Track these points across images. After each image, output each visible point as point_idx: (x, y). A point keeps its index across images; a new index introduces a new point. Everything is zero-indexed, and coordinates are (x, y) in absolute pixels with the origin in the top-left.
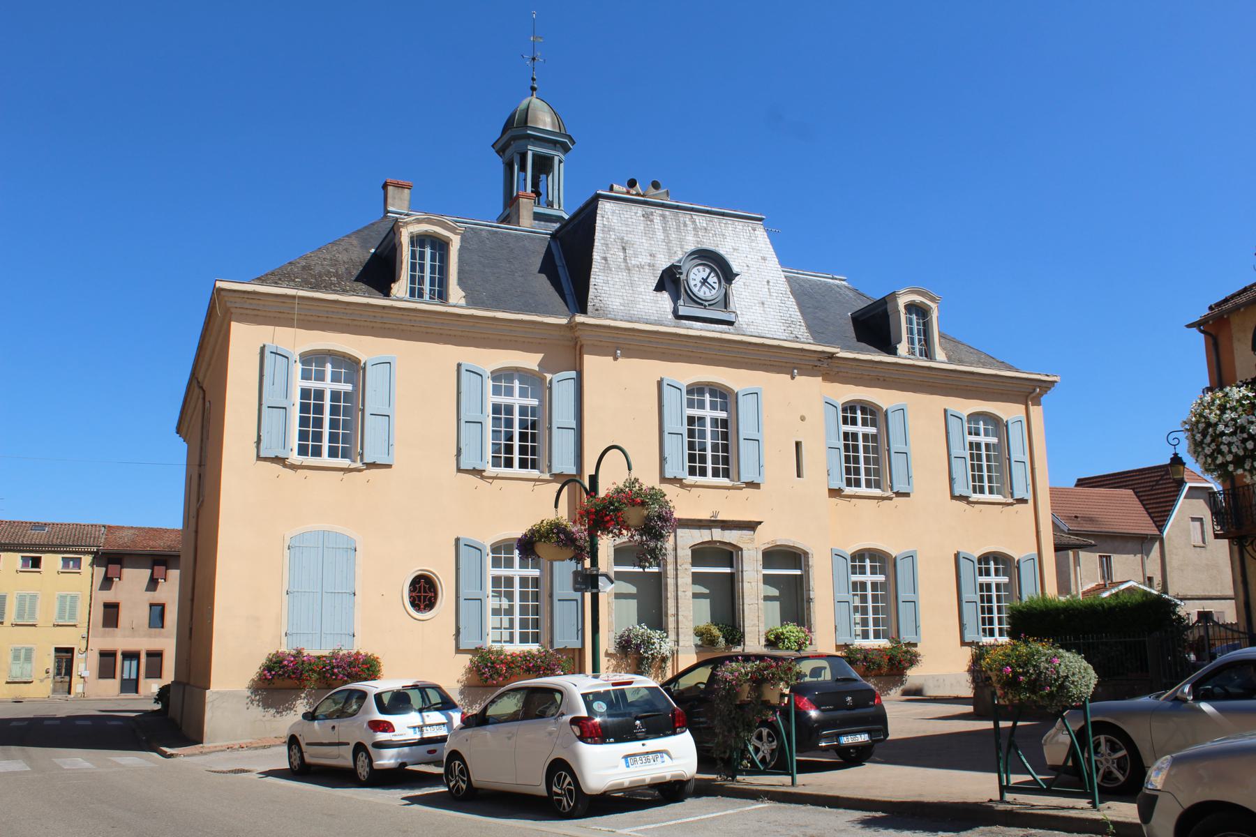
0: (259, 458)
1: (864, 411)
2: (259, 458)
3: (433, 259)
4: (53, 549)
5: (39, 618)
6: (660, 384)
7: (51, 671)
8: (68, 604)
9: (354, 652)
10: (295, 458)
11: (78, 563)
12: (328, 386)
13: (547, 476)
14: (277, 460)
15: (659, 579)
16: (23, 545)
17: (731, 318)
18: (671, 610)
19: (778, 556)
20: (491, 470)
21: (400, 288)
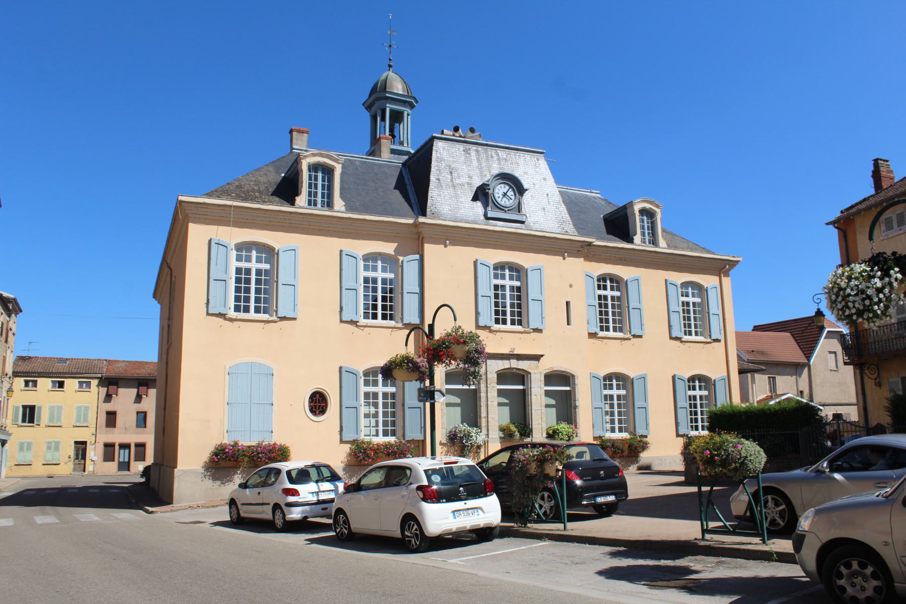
0: (208, 314)
1: (612, 281)
3: (323, 180)
4: (72, 375)
5: (64, 421)
6: (475, 263)
8: (82, 412)
9: (272, 443)
10: (232, 314)
11: (89, 385)
15: (475, 394)
16: (52, 373)
18: (483, 414)
19: (553, 378)
20: (363, 321)
21: (302, 200)
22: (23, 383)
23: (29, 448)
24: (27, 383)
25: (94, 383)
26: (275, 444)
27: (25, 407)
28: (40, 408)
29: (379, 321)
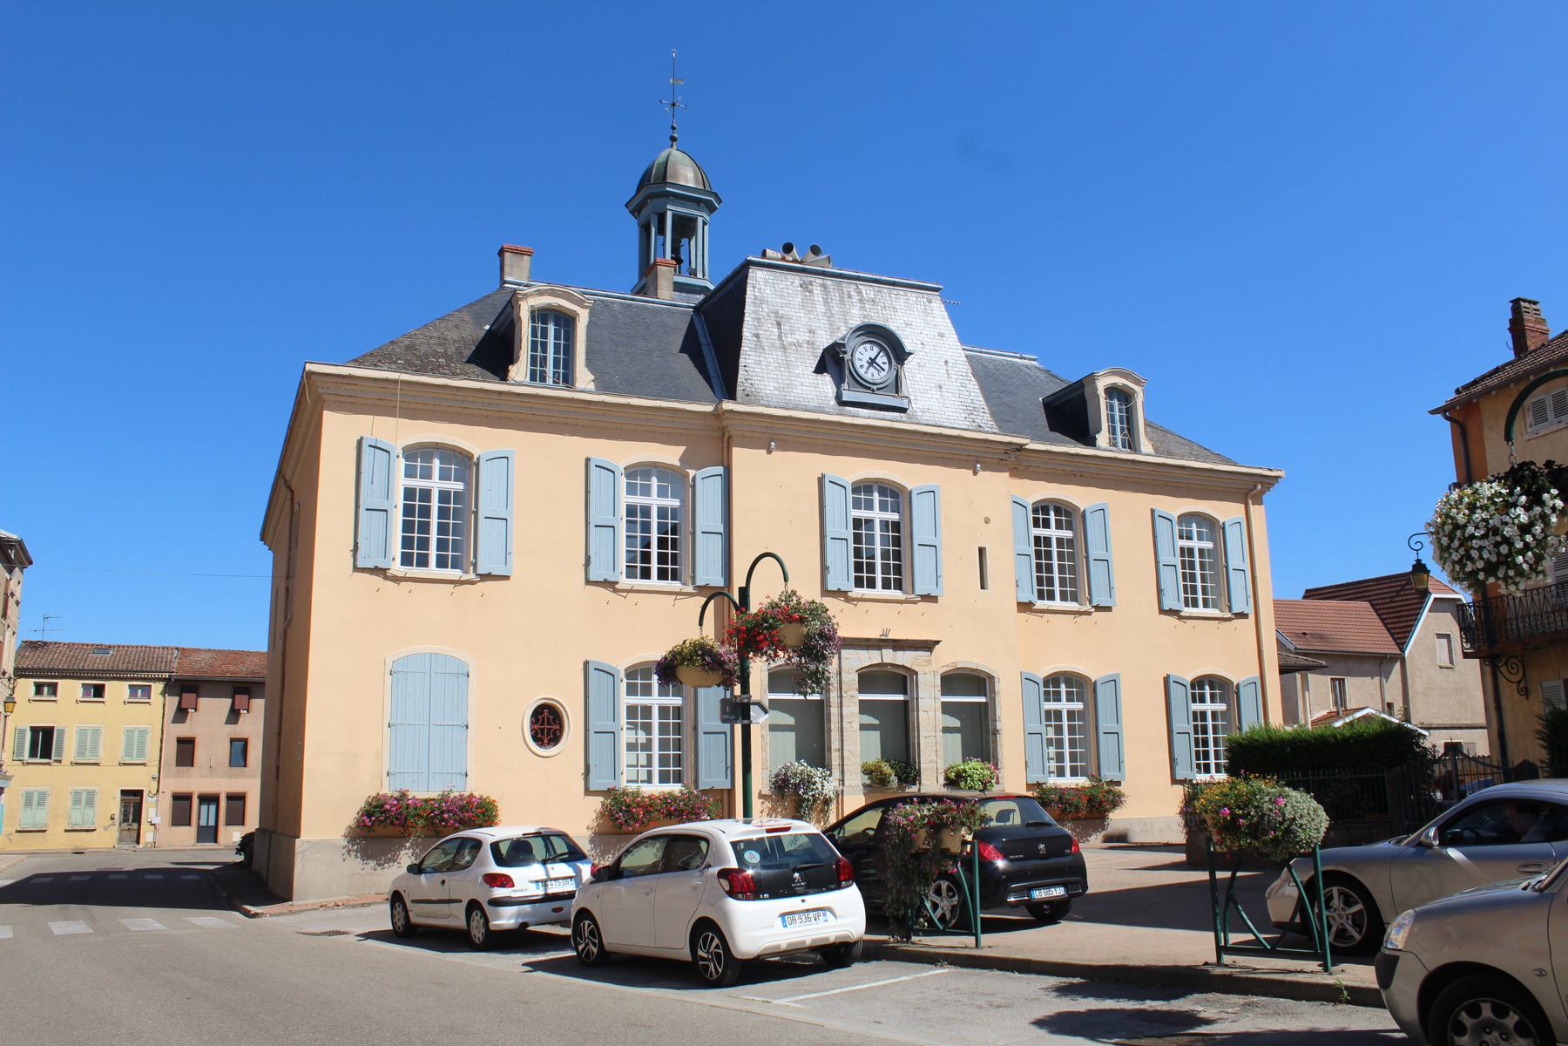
1: (1058, 511)
3: (557, 337)
4: (118, 675)
5: (103, 755)
6: (821, 480)
8: (135, 740)
9: (466, 794)
10: (397, 568)
11: (147, 691)
12: (436, 485)
13: (690, 589)
15: (821, 708)
16: (84, 670)
17: (904, 404)
18: (835, 745)
19: (956, 680)
20: (625, 582)
21: (519, 371)
23: (41, 803)
24: (39, 689)
25: (157, 688)
26: (471, 796)
27: (35, 730)
28: (62, 732)
29: (432, 570)
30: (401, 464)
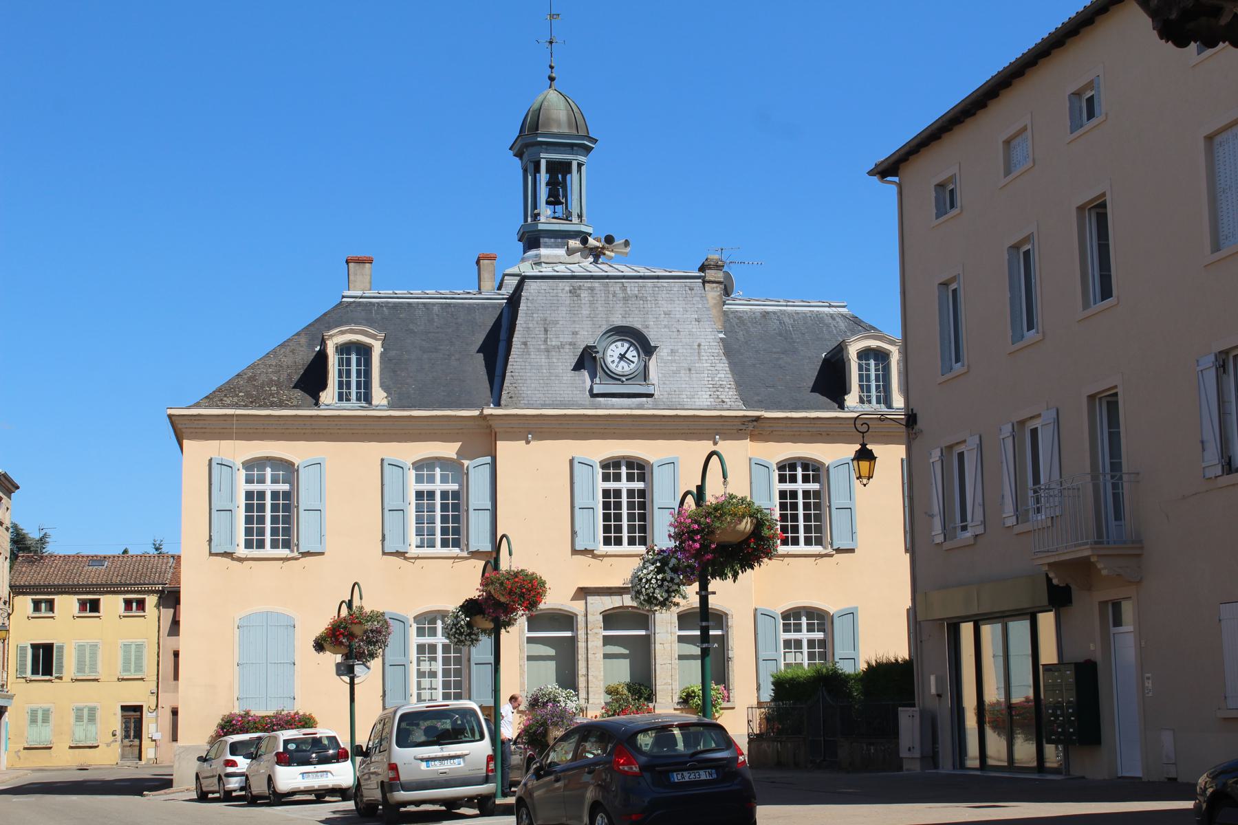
0: (211, 554)
1: (805, 467)
2: (211, 554)
3: (358, 364)
4: (113, 589)
5: (102, 671)
6: (572, 461)
7: (119, 733)
8: (132, 654)
9: (292, 713)
10: (241, 551)
11: (141, 604)
12: (268, 487)
13: (465, 554)
14: (585, 552)
15: (573, 641)
16: (78, 585)
17: (650, 390)
18: (582, 670)
20: (413, 551)
21: (329, 396)
22: (31, 605)
23: (46, 720)
24: (37, 605)
25: (151, 601)
26: (297, 713)
27: (35, 647)
28: (61, 648)
29: (439, 550)
30: (242, 474)
